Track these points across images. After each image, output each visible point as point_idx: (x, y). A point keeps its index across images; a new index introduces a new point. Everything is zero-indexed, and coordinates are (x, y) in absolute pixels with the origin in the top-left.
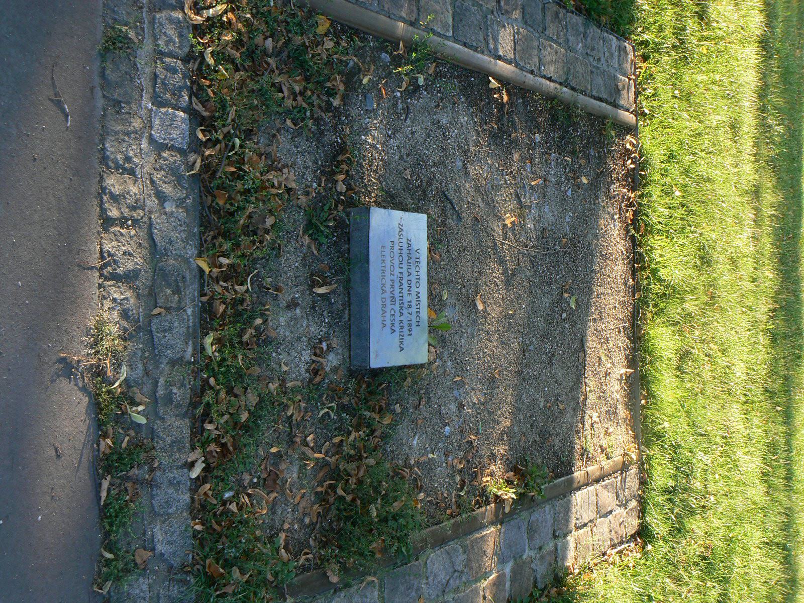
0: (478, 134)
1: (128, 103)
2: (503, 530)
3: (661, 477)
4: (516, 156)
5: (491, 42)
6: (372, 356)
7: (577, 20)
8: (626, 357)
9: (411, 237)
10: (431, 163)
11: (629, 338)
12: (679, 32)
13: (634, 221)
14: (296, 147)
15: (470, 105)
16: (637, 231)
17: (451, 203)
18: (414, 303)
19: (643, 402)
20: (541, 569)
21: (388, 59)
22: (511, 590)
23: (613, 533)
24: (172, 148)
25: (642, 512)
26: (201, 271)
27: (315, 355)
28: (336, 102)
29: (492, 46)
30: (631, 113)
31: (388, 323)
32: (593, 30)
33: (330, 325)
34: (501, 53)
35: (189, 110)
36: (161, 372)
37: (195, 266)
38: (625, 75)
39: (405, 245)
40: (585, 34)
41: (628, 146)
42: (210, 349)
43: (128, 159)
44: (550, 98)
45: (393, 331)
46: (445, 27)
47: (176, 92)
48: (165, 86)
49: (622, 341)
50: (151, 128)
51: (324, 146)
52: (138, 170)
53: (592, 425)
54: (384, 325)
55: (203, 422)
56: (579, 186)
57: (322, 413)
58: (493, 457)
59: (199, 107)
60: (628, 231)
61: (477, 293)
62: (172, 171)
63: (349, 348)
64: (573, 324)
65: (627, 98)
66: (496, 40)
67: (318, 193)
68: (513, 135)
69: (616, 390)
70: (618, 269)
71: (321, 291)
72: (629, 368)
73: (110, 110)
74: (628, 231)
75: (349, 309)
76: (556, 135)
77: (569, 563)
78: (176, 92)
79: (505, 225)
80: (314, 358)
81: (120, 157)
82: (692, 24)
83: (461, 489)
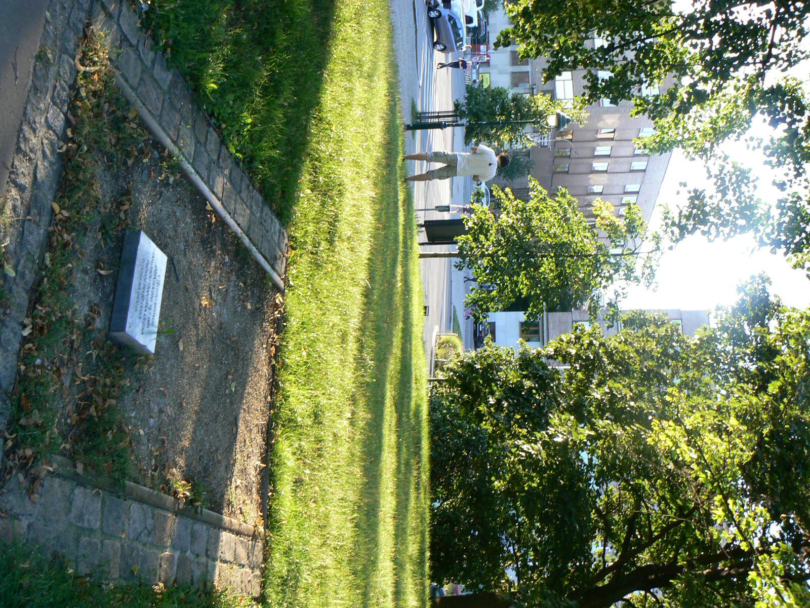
0: (195, 234)
1: (41, 92)
2: (177, 521)
3: (279, 565)
4: (213, 264)
5: (211, 180)
6: (128, 325)
7: (259, 198)
8: (261, 454)
9: (158, 265)
10: (168, 235)
11: (264, 440)
12: (316, 244)
13: (276, 356)
14: (105, 176)
15: (194, 213)
16: (278, 362)
17: (175, 269)
18: (153, 308)
19: (270, 494)
20: (197, 573)
21: (157, 156)
22: (177, 573)
23: (243, 585)
24: (54, 131)
25: (263, 586)
26: (53, 210)
27: (91, 311)
28: (130, 162)
29: (211, 183)
30: (282, 279)
31: (139, 310)
32: (266, 209)
33: (101, 299)
34: (215, 190)
35: (65, 115)
36: (22, 256)
37: (50, 207)
38: (281, 251)
39: (154, 269)
40: (262, 209)
41: (277, 301)
42: (48, 262)
43: (35, 122)
44: (236, 237)
45: (140, 318)
46: (189, 154)
47: (63, 104)
48: (59, 95)
49: (259, 439)
50: (48, 113)
51: (118, 185)
52: (37, 131)
53: (236, 487)
54: (136, 310)
55: (35, 303)
56: (245, 308)
57: (88, 352)
58: (175, 465)
59: (71, 117)
60: (270, 362)
61: (180, 338)
62: (52, 144)
63: (110, 319)
64: (232, 403)
65: (281, 267)
66: (214, 181)
67: (110, 211)
68: (214, 247)
69: (253, 476)
70: (263, 385)
71: (102, 272)
72: (262, 463)
73: (32, 91)
74: (270, 362)
75: (114, 295)
76: (237, 265)
77: (216, 583)
78: (63, 104)
79: (201, 304)
80: (90, 313)
81: (31, 118)
82: (324, 245)
83: (155, 470)
